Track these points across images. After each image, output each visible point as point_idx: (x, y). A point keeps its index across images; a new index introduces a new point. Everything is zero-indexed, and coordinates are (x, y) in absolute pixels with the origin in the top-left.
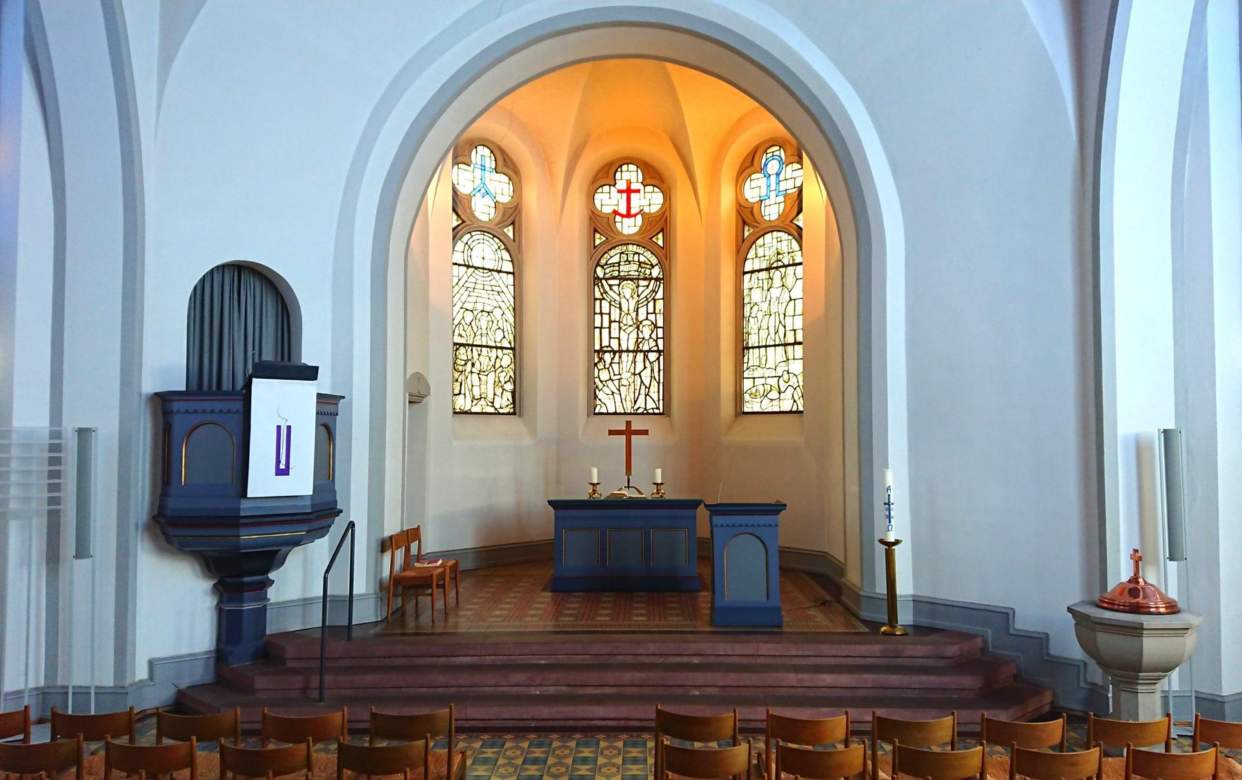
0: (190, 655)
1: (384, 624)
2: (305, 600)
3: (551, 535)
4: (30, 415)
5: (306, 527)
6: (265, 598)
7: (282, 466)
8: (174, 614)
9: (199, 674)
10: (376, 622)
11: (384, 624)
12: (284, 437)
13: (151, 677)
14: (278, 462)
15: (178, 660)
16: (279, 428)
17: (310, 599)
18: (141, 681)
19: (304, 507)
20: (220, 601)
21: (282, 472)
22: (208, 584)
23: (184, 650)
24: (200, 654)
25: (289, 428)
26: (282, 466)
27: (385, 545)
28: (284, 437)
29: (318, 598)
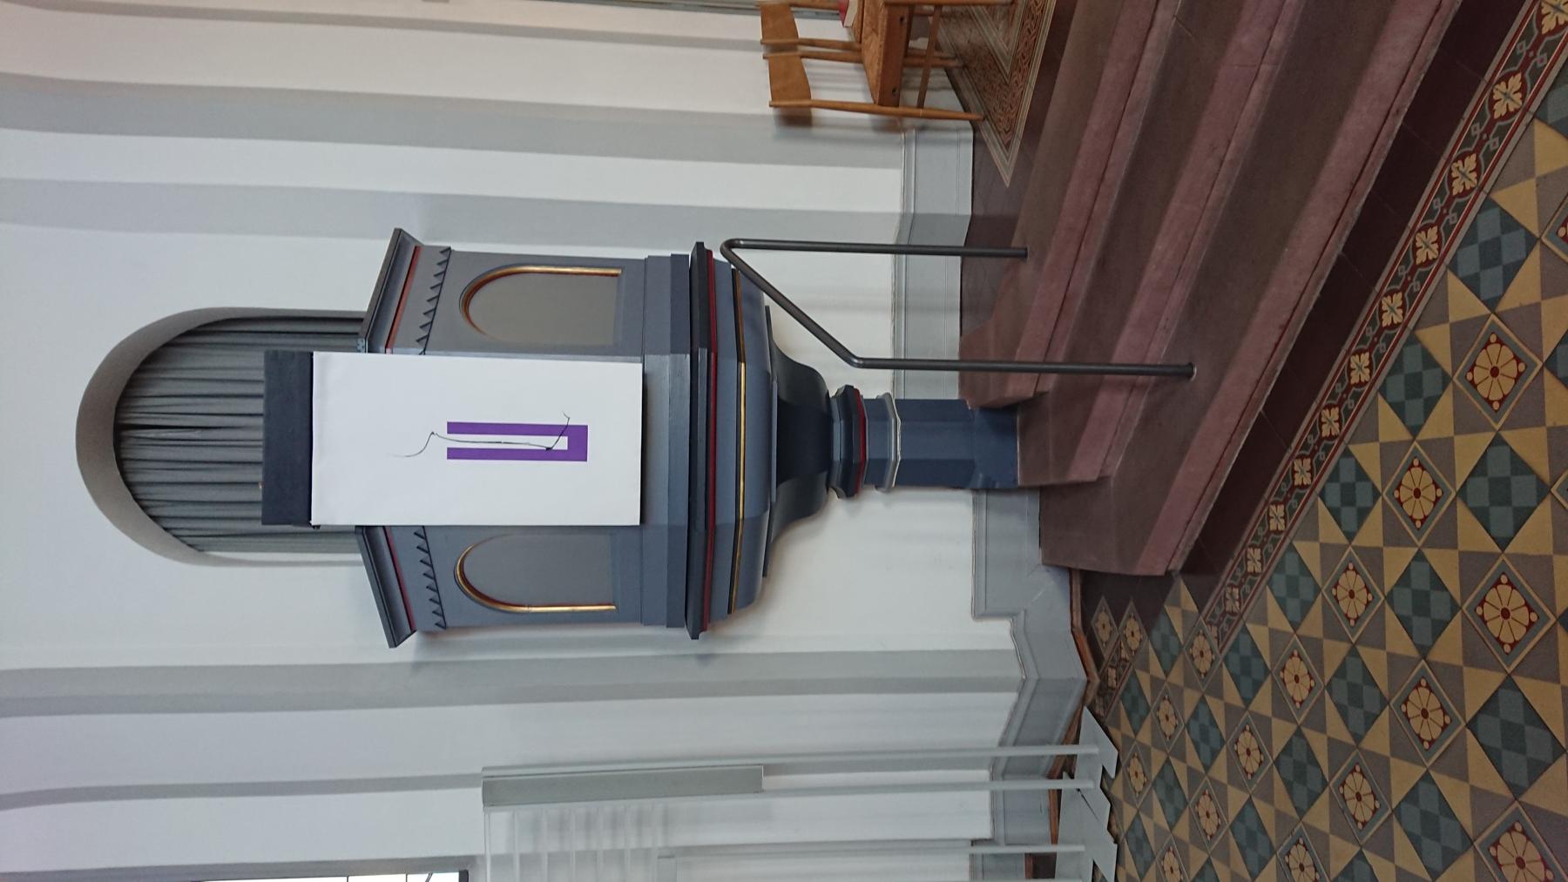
0: (976, 540)
1: (986, 126)
2: (896, 308)
3: (1029, 506)
4: (463, 823)
5: (728, 363)
6: (880, 403)
7: (562, 443)
8: (898, 580)
9: (1018, 524)
10: (976, 142)
11: (986, 126)
12: (477, 441)
13: (1011, 615)
14: (549, 454)
15: (983, 564)
16: (454, 454)
17: (896, 294)
18: (1014, 635)
19: (676, 373)
20: (879, 484)
21: (577, 442)
22: (838, 510)
23: (966, 551)
24: (976, 521)
25: (454, 428)
26: (562, 443)
27: (796, 116)
28: (477, 441)
29: (896, 265)
